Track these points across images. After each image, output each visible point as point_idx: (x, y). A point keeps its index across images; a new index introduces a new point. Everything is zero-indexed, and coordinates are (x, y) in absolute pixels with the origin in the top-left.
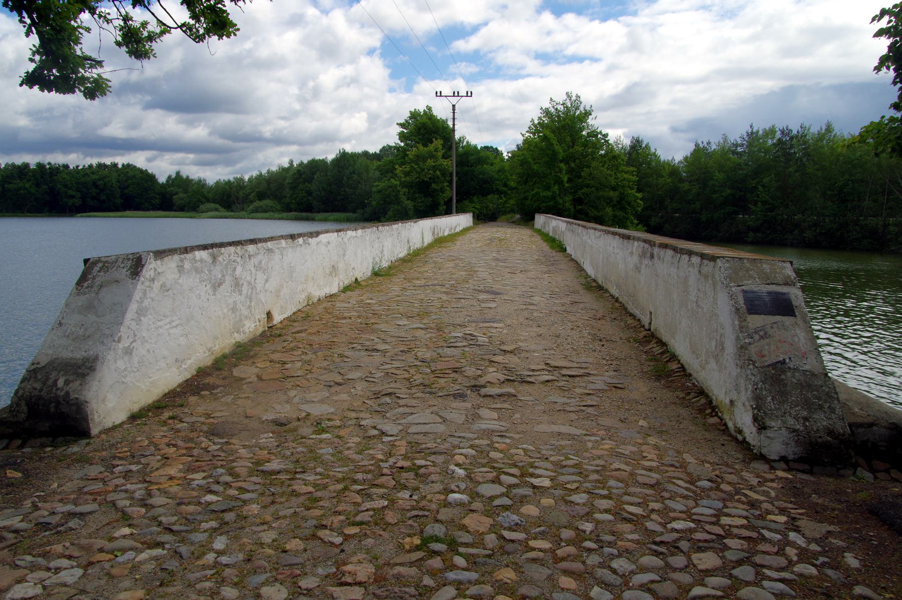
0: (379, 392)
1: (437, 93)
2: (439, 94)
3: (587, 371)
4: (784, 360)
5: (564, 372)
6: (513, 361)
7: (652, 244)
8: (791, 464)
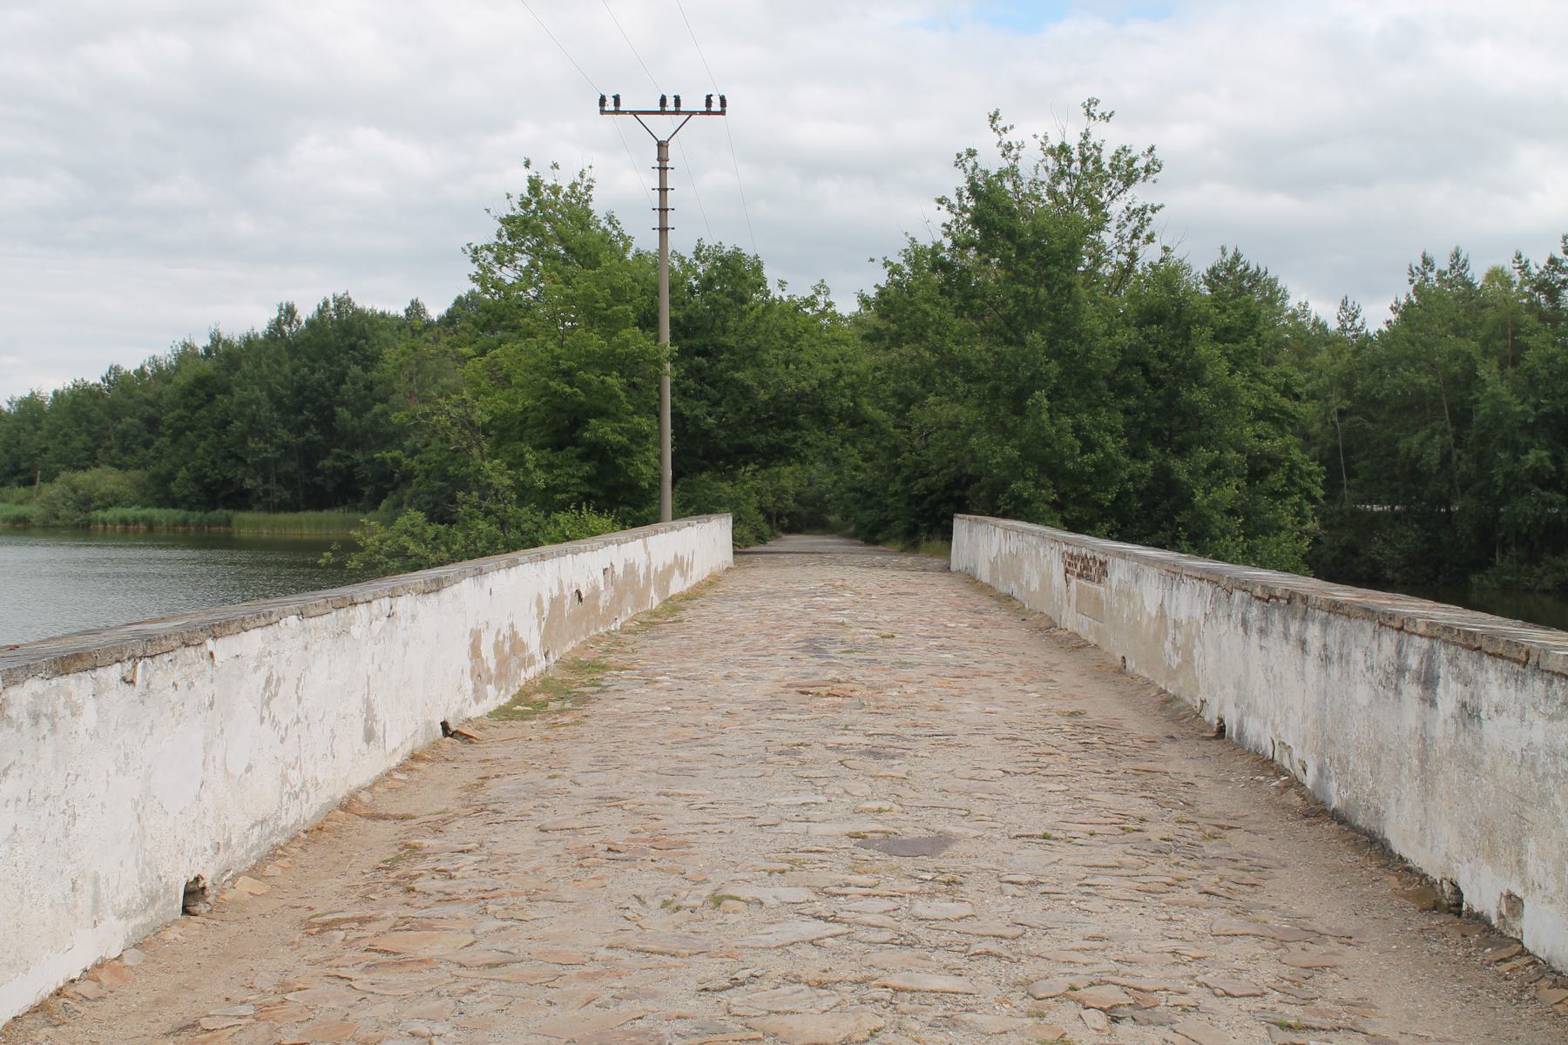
2: (610, 106)
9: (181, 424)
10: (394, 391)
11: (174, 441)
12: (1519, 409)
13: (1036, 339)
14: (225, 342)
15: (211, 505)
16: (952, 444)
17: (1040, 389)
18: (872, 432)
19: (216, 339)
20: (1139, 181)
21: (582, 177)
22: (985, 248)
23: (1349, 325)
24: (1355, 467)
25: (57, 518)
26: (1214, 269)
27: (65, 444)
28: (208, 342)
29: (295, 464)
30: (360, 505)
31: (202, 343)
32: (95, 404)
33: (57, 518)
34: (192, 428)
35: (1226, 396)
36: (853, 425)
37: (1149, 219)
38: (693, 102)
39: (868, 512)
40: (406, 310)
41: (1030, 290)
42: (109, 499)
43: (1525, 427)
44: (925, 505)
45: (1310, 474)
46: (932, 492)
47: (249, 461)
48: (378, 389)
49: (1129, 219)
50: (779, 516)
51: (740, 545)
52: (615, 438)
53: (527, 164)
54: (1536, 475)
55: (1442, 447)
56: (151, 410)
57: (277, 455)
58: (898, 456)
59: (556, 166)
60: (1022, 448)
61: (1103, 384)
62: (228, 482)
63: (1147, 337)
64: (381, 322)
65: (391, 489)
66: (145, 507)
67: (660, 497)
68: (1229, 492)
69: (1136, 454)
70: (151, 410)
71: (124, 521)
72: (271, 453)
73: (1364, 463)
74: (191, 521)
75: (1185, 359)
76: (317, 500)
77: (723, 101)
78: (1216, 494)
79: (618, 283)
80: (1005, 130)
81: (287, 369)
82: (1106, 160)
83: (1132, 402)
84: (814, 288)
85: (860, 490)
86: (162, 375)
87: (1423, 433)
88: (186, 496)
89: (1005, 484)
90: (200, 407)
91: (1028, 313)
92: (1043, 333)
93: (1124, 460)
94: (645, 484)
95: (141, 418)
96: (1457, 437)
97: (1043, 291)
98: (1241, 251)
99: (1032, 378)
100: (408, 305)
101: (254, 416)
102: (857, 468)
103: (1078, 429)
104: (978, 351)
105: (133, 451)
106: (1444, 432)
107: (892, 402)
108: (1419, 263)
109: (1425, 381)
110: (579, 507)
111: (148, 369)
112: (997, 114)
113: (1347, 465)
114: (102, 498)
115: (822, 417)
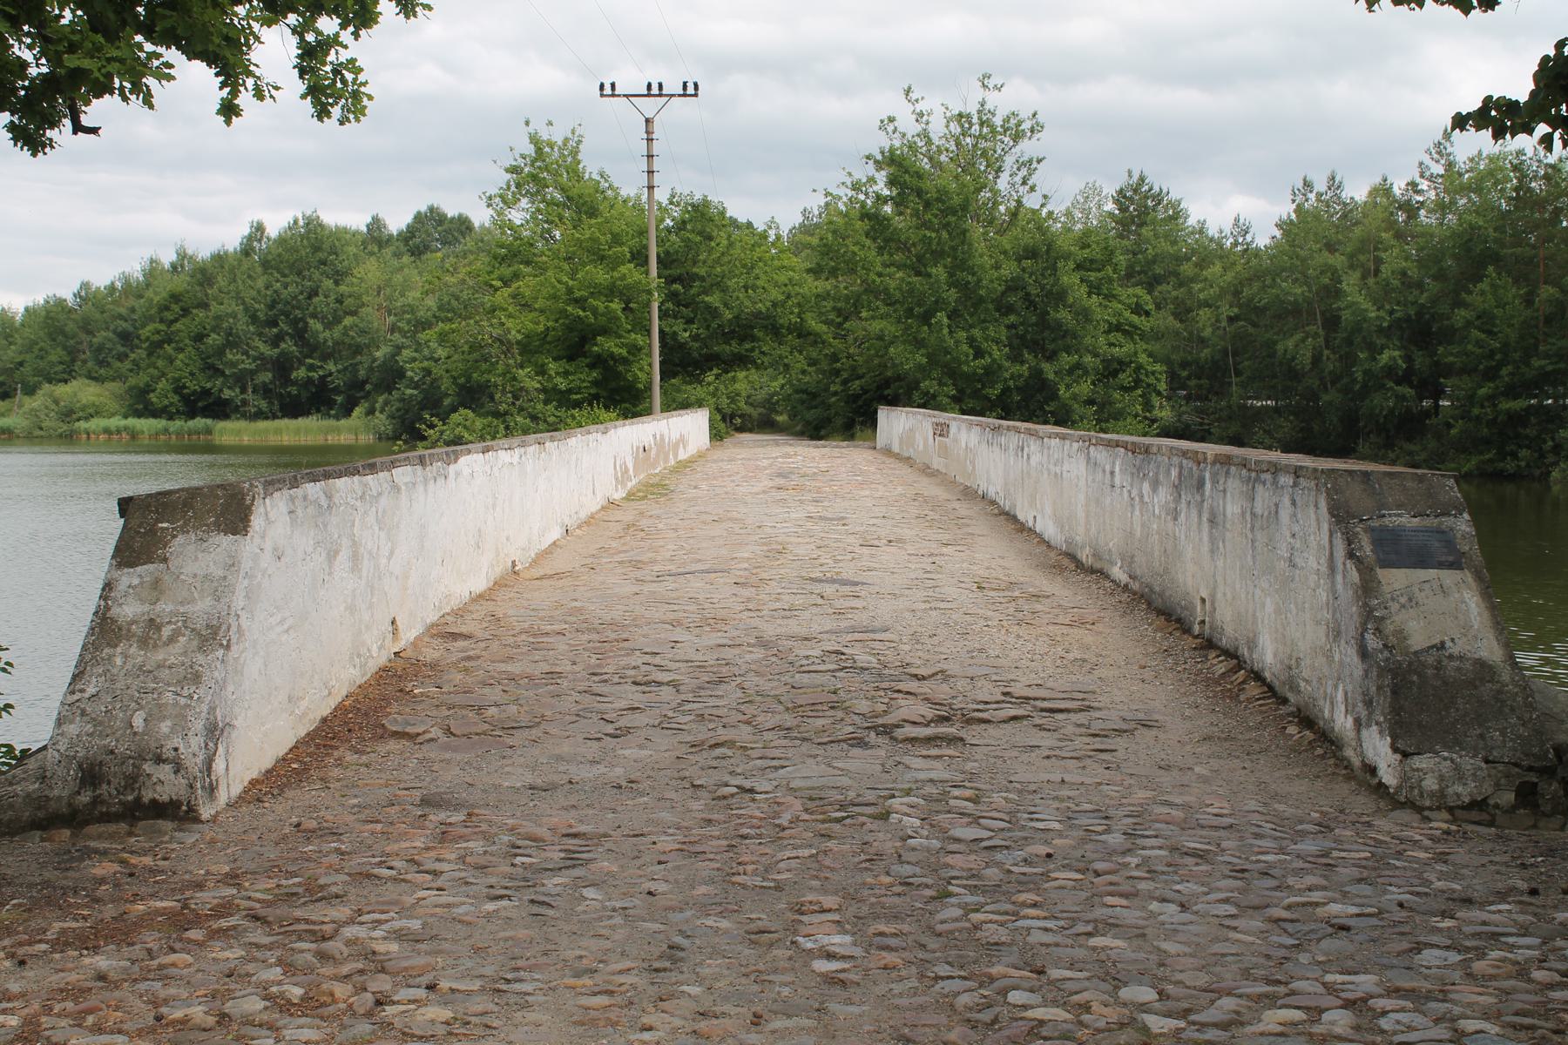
0: (703, 743)
1: (602, 87)
2: (608, 91)
3: (1087, 703)
4: (1443, 643)
5: (1040, 704)
6: (942, 691)
7: (1199, 459)
8: (1458, 812)
9: (157, 338)
10: (363, 305)
11: (150, 355)
12: (1373, 315)
13: (939, 272)
14: (191, 257)
15: (191, 415)
16: (877, 352)
17: (941, 310)
18: (816, 342)
19: (182, 255)
20: (1026, 140)
21: (573, 133)
22: (899, 202)
23: (1240, 240)
24: (1240, 367)
25: (41, 429)
26: (1121, 190)
27: (42, 358)
28: (174, 257)
29: (270, 375)
30: (333, 412)
31: (168, 258)
32: (69, 319)
33: (41, 429)
34: (170, 341)
35: (1085, 315)
36: (799, 336)
37: (1035, 169)
38: (673, 87)
39: (812, 411)
40: (368, 226)
41: (934, 235)
42: (91, 411)
43: (1380, 330)
44: (860, 403)
45: (1153, 373)
46: (866, 392)
47: (227, 373)
48: (348, 301)
49: (1019, 169)
50: (732, 416)
51: (716, 435)
52: (616, 350)
53: (527, 123)
54: (1390, 371)
55: (1314, 348)
56: (125, 325)
57: (253, 366)
58: (838, 360)
59: (550, 123)
60: (929, 356)
61: (991, 306)
62: (206, 393)
63: (1024, 270)
64: (341, 234)
65: (362, 398)
66: (126, 417)
67: (650, 397)
68: (1085, 388)
69: (1016, 358)
70: (125, 325)
71: (107, 431)
72: (248, 365)
73: (1246, 363)
74: (171, 430)
75: (1053, 286)
76: (293, 409)
77: (696, 86)
78: (1076, 389)
79: (616, 229)
80: (917, 101)
81: (260, 283)
82: (998, 121)
83: (1012, 318)
84: (766, 224)
85: (804, 391)
86: (130, 289)
87: (1298, 336)
88: (167, 406)
89: (918, 383)
90: (176, 320)
91: (933, 252)
92: (945, 267)
93: (1007, 364)
94: (641, 386)
95: (114, 332)
96: (1327, 341)
97: (945, 235)
98: (1146, 173)
99: (936, 302)
100: (369, 220)
101: (231, 329)
102: (804, 372)
103: (971, 341)
104: (896, 280)
105: (109, 364)
106: (1316, 335)
107: (832, 316)
108: (1300, 185)
109: (1299, 291)
110: (591, 404)
111: (119, 285)
112: (910, 88)
113: (1235, 364)
114: (83, 409)
115: (775, 331)
